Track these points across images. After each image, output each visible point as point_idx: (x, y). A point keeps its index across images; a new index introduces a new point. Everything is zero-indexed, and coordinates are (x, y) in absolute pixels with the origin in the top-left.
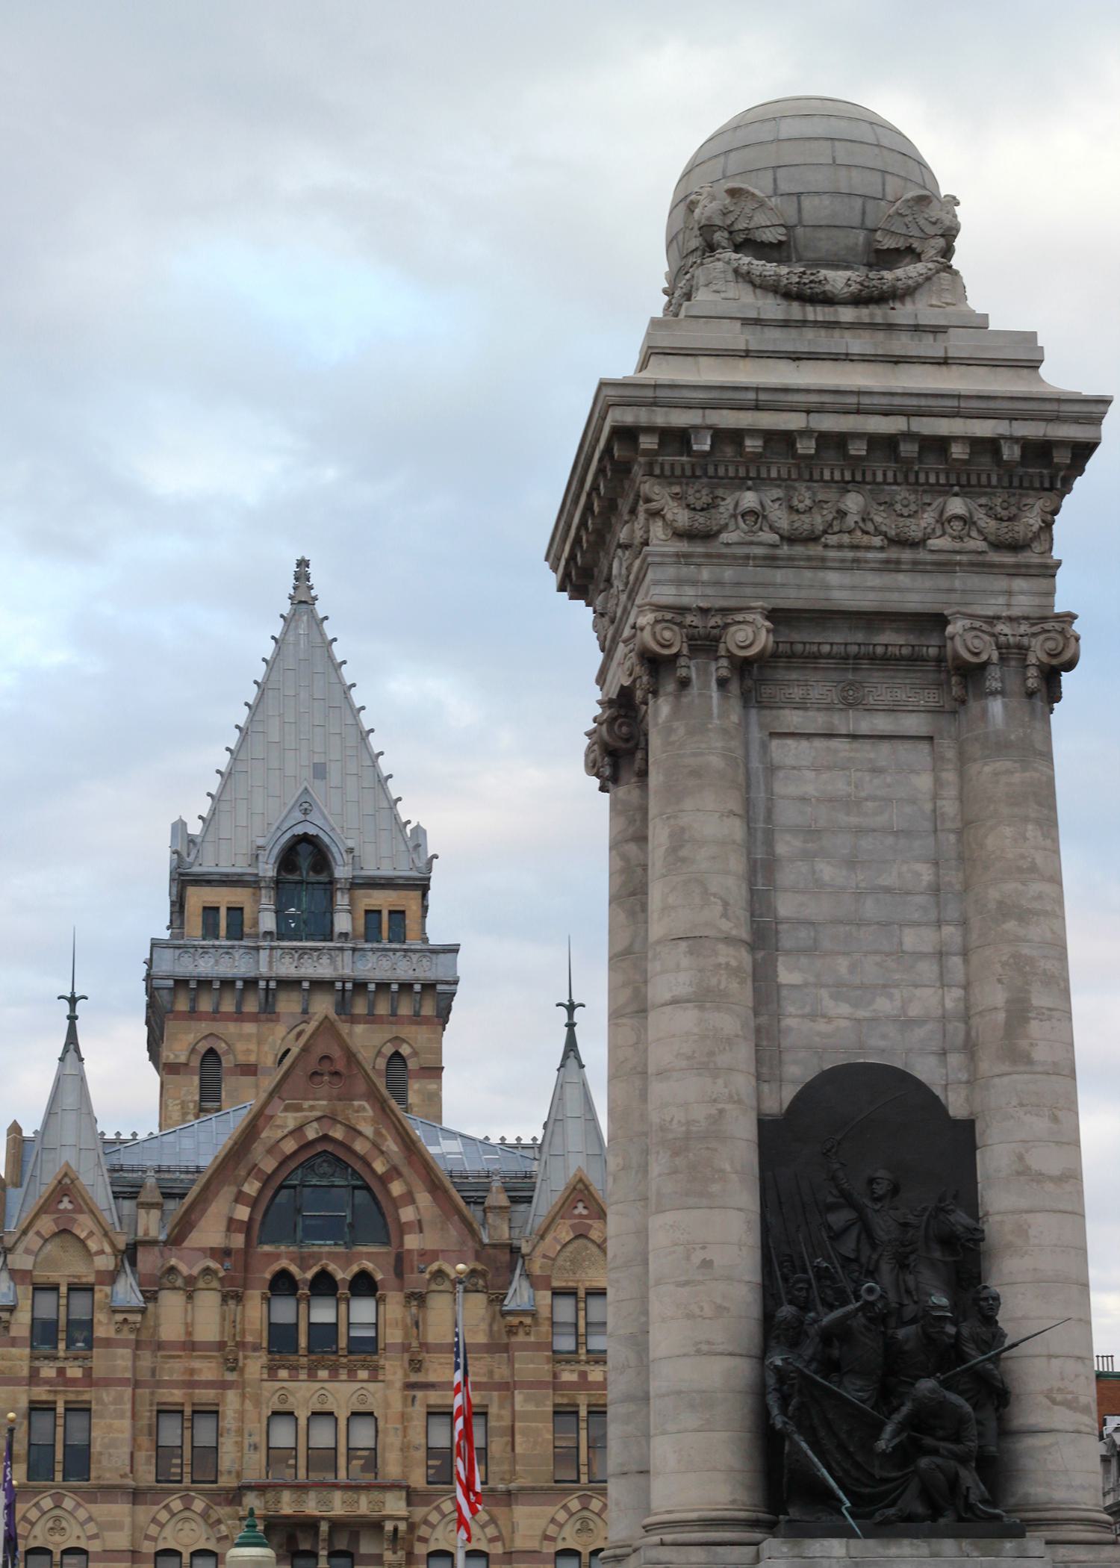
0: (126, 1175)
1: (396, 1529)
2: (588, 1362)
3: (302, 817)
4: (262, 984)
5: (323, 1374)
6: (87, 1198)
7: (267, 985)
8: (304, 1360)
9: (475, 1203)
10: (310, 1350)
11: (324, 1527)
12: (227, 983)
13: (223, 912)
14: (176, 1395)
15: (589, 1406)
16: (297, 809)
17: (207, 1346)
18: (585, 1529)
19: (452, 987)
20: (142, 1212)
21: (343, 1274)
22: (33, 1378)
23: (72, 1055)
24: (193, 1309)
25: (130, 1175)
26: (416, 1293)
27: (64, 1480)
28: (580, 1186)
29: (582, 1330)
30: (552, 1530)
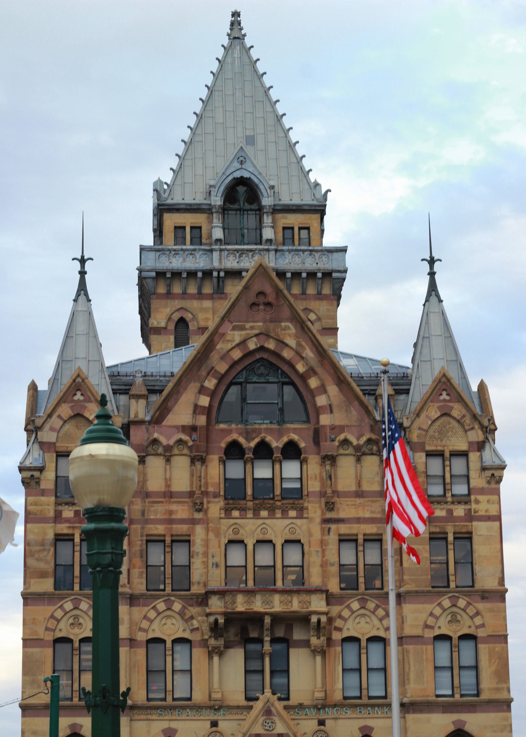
0: (122, 378)
1: (319, 621)
2: (453, 503)
3: (239, 166)
4: (215, 274)
5: (264, 513)
6: (93, 391)
7: (219, 274)
8: (250, 504)
9: (369, 394)
10: (254, 498)
11: (267, 620)
12: (192, 274)
13: (188, 229)
14: (160, 529)
15: (454, 533)
16: (236, 161)
17: (181, 494)
18: (454, 620)
19: (343, 274)
20: (133, 401)
21: (276, 444)
22: (58, 518)
23: (82, 298)
24: (170, 468)
25: (125, 378)
26: (329, 456)
27: (80, 589)
28: (444, 379)
29: (448, 480)
30: (431, 621)
